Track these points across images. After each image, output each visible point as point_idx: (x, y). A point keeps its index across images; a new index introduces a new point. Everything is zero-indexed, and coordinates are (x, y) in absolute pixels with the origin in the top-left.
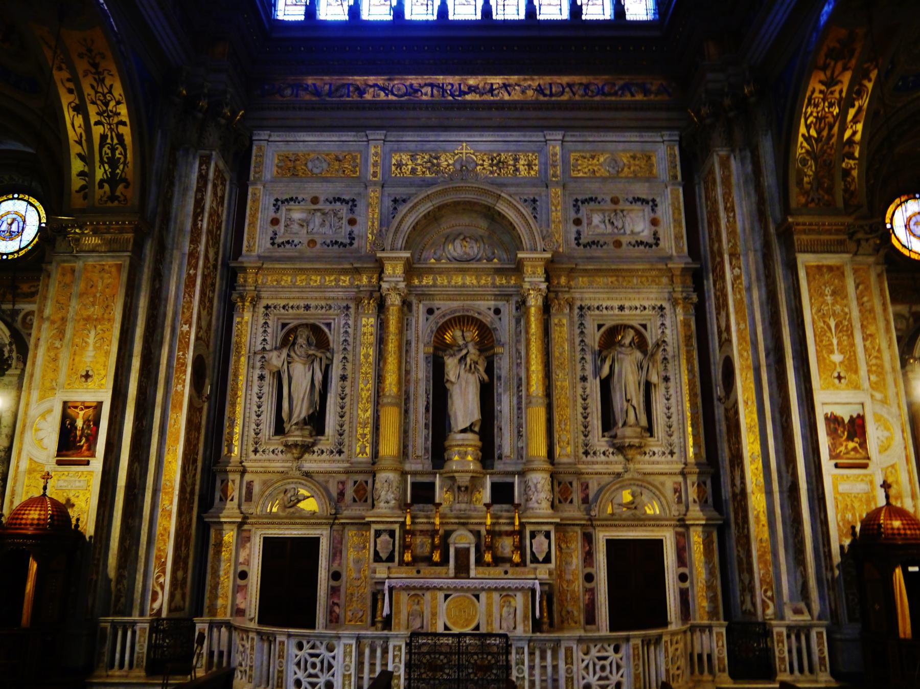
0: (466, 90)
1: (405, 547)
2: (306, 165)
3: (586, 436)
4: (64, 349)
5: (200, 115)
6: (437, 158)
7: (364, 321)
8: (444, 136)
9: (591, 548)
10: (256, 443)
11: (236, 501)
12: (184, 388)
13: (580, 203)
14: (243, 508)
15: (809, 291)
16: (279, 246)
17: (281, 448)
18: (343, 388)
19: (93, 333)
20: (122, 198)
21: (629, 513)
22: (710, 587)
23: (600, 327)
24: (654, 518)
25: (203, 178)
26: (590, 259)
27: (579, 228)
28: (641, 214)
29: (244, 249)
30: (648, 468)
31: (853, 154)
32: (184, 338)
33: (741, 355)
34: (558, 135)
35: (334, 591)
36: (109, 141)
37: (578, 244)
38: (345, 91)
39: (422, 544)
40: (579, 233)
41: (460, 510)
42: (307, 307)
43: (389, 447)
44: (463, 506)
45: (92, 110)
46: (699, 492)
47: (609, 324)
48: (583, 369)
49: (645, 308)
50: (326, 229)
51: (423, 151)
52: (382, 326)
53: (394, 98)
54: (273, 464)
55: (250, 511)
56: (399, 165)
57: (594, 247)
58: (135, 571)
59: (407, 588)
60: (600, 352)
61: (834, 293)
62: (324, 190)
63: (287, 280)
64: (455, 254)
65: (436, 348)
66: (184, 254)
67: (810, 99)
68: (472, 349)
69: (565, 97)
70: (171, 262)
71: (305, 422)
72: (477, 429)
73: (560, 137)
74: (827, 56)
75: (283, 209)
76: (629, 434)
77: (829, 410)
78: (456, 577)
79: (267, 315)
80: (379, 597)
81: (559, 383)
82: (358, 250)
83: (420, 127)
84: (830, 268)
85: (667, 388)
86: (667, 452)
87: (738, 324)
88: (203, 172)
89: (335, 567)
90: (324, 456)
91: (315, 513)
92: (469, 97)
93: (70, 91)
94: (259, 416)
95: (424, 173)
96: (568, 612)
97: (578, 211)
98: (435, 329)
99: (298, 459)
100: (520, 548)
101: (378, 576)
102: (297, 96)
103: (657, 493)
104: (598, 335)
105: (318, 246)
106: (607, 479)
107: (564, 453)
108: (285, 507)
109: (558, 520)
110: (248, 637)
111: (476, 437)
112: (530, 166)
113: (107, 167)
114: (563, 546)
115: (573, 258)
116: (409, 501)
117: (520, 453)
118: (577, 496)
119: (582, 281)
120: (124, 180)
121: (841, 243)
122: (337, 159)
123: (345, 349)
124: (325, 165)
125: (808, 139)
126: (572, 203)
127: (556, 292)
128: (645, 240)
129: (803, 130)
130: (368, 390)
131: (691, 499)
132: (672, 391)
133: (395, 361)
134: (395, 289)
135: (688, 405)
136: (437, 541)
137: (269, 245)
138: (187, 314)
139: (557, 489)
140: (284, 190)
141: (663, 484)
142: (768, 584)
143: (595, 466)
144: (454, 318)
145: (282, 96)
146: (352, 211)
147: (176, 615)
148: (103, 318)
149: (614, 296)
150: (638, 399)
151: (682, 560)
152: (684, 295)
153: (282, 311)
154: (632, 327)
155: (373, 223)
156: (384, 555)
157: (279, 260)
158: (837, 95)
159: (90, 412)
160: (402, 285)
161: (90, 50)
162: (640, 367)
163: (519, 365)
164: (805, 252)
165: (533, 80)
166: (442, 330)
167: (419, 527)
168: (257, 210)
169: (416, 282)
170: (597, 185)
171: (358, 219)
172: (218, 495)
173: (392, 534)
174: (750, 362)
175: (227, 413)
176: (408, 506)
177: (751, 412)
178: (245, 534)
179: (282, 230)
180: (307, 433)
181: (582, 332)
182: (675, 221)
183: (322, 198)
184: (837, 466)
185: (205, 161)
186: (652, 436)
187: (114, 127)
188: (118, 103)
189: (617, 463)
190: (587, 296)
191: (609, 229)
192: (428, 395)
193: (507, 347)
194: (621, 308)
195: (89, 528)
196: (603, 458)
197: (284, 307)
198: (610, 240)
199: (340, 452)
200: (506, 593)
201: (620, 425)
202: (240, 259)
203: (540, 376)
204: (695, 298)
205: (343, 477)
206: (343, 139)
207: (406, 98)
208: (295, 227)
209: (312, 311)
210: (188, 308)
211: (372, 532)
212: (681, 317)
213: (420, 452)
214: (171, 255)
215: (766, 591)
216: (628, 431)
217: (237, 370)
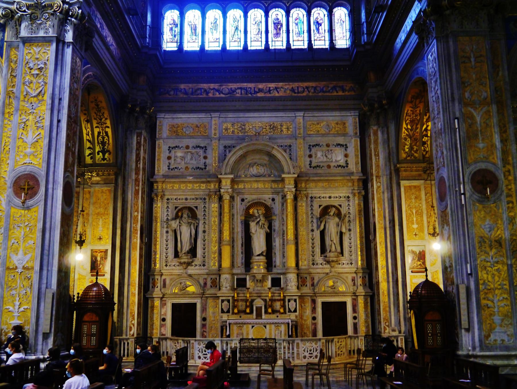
0: (257, 91)
1: (234, 307)
2: (182, 129)
3: (313, 256)
4: (89, 227)
5: (136, 114)
6: (244, 125)
7: (213, 205)
8: (248, 115)
9: (315, 306)
10: (166, 262)
11: (159, 288)
13: (311, 147)
14: (162, 290)
15: (405, 197)
16: (172, 170)
17: (177, 264)
18: (204, 236)
19: (101, 220)
20: (108, 159)
21: (332, 290)
22: (366, 322)
23: (320, 206)
24: (343, 293)
25: (139, 143)
26: (316, 175)
27: (311, 159)
28: (340, 151)
29: (156, 172)
30: (341, 270)
31: (427, 134)
32: (136, 218)
33: (379, 222)
34: (301, 114)
35: (204, 326)
36: (101, 134)
37: (311, 167)
38: (199, 92)
39: (241, 305)
40: (311, 162)
41: (258, 290)
42: (186, 199)
43: (226, 263)
44: (259, 288)
46: (363, 281)
47: (324, 204)
48: (312, 226)
49: (341, 197)
50: (194, 162)
51: (238, 122)
52: (221, 207)
53: (223, 96)
54: (174, 271)
55: (166, 292)
56: (226, 129)
57: (318, 168)
59: (236, 324)
60: (320, 218)
61: (416, 198)
62: (192, 142)
63: (176, 186)
64: (254, 173)
65: (245, 217)
66: (133, 180)
67: (407, 114)
68: (262, 218)
69: (305, 94)
70: (128, 185)
71: (188, 252)
72: (264, 254)
73: (302, 115)
74: (412, 98)
75: (173, 151)
76: (332, 256)
77: (410, 248)
78: (256, 319)
79: (168, 203)
80: (224, 327)
81: (301, 233)
82: (208, 172)
83: (235, 110)
84: (415, 187)
85: (350, 234)
86: (349, 263)
87: (378, 208)
88: (139, 141)
89: (204, 316)
91: (194, 292)
92: (259, 95)
93: (85, 114)
94: (167, 249)
95: (238, 133)
96: (305, 333)
97: (310, 151)
98: (245, 208)
99: (186, 268)
100: (284, 306)
101: (223, 319)
102: (176, 95)
103: (344, 282)
104: (319, 210)
105: (190, 170)
106: (321, 276)
107: (303, 264)
108: (181, 290)
109: (300, 294)
110: (178, 343)
111: (264, 258)
112: (288, 129)
113: (101, 145)
114: (303, 305)
115: (308, 174)
116: (236, 287)
117: (284, 264)
118: (309, 283)
119: (312, 185)
120: (108, 151)
121: (420, 175)
122: (197, 126)
123: (204, 218)
124: (191, 130)
125: (407, 129)
126: (308, 147)
127: (300, 191)
128: (342, 164)
129: (404, 125)
130: (216, 237)
131: (359, 284)
132: (352, 235)
133: (228, 225)
134: (227, 192)
135: (359, 242)
136: (248, 304)
137: (167, 170)
138: (136, 207)
139: (300, 280)
140: (172, 143)
141: (347, 277)
142: (387, 320)
143: (318, 270)
144: (254, 203)
145: (170, 95)
146: (205, 152)
147: (139, 336)
148: (105, 213)
149: (326, 192)
150: (336, 240)
151: (355, 310)
152: (358, 191)
153: (175, 201)
154: (334, 206)
155: (215, 158)
156: (225, 310)
157: (173, 177)
158: (418, 112)
160: (230, 190)
161: (96, 100)
162: (338, 225)
163: (283, 224)
164: (404, 180)
165: (290, 85)
166: (248, 208)
167: (240, 298)
168: (161, 152)
169: (236, 187)
170: (320, 138)
171: (208, 156)
172: (151, 286)
173: (229, 301)
174: (383, 225)
175: (153, 249)
176: (235, 289)
177: (382, 247)
178: (164, 302)
179: (173, 162)
180: (189, 257)
181: (312, 209)
182: (355, 155)
183: (191, 146)
184: (412, 272)
185: (139, 135)
186: (343, 256)
187: (104, 128)
188: (106, 119)
189: (327, 268)
190: (314, 192)
191: (325, 159)
192: (242, 239)
193: (278, 216)
194: (330, 197)
196: (321, 266)
197: (176, 199)
198: (325, 164)
199: (204, 265)
200: (277, 325)
201: (328, 251)
202: (154, 177)
203: (292, 231)
204: (363, 193)
205: (206, 276)
206: (200, 116)
207: (229, 95)
208: (179, 160)
209: (189, 201)
210: (136, 205)
211: (220, 301)
212: (357, 202)
213: (239, 265)
214: (128, 181)
215: (386, 323)
216: (332, 254)
217: (156, 229)
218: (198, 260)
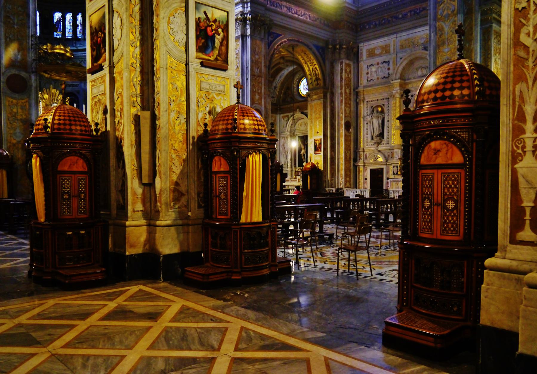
5: (337, 51)
12: (343, 131)
18: (388, 124)
25: (342, 69)
45: (308, 63)
58: (335, 178)
71: (378, 136)
90: (384, 145)
146: (388, 65)
156: (395, 173)
159: (319, 141)
172: (358, 158)
173: (397, 167)
183: (380, 62)
185: (342, 63)
195: (322, 169)
218: (384, 141)
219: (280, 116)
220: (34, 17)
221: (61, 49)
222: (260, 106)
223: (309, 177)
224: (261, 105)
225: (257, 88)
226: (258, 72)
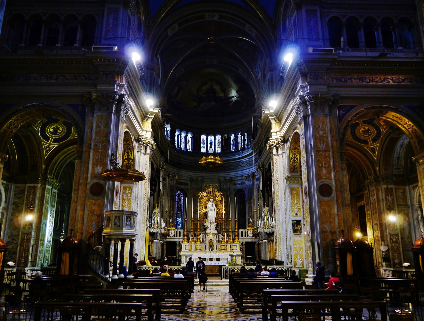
219: (409, 187)
220: (116, 141)
221: (211, 159)
222: (330, 181)
223: (420, 256)
224: (331, 180)
225: (323, 163)
226: (324, 147)
